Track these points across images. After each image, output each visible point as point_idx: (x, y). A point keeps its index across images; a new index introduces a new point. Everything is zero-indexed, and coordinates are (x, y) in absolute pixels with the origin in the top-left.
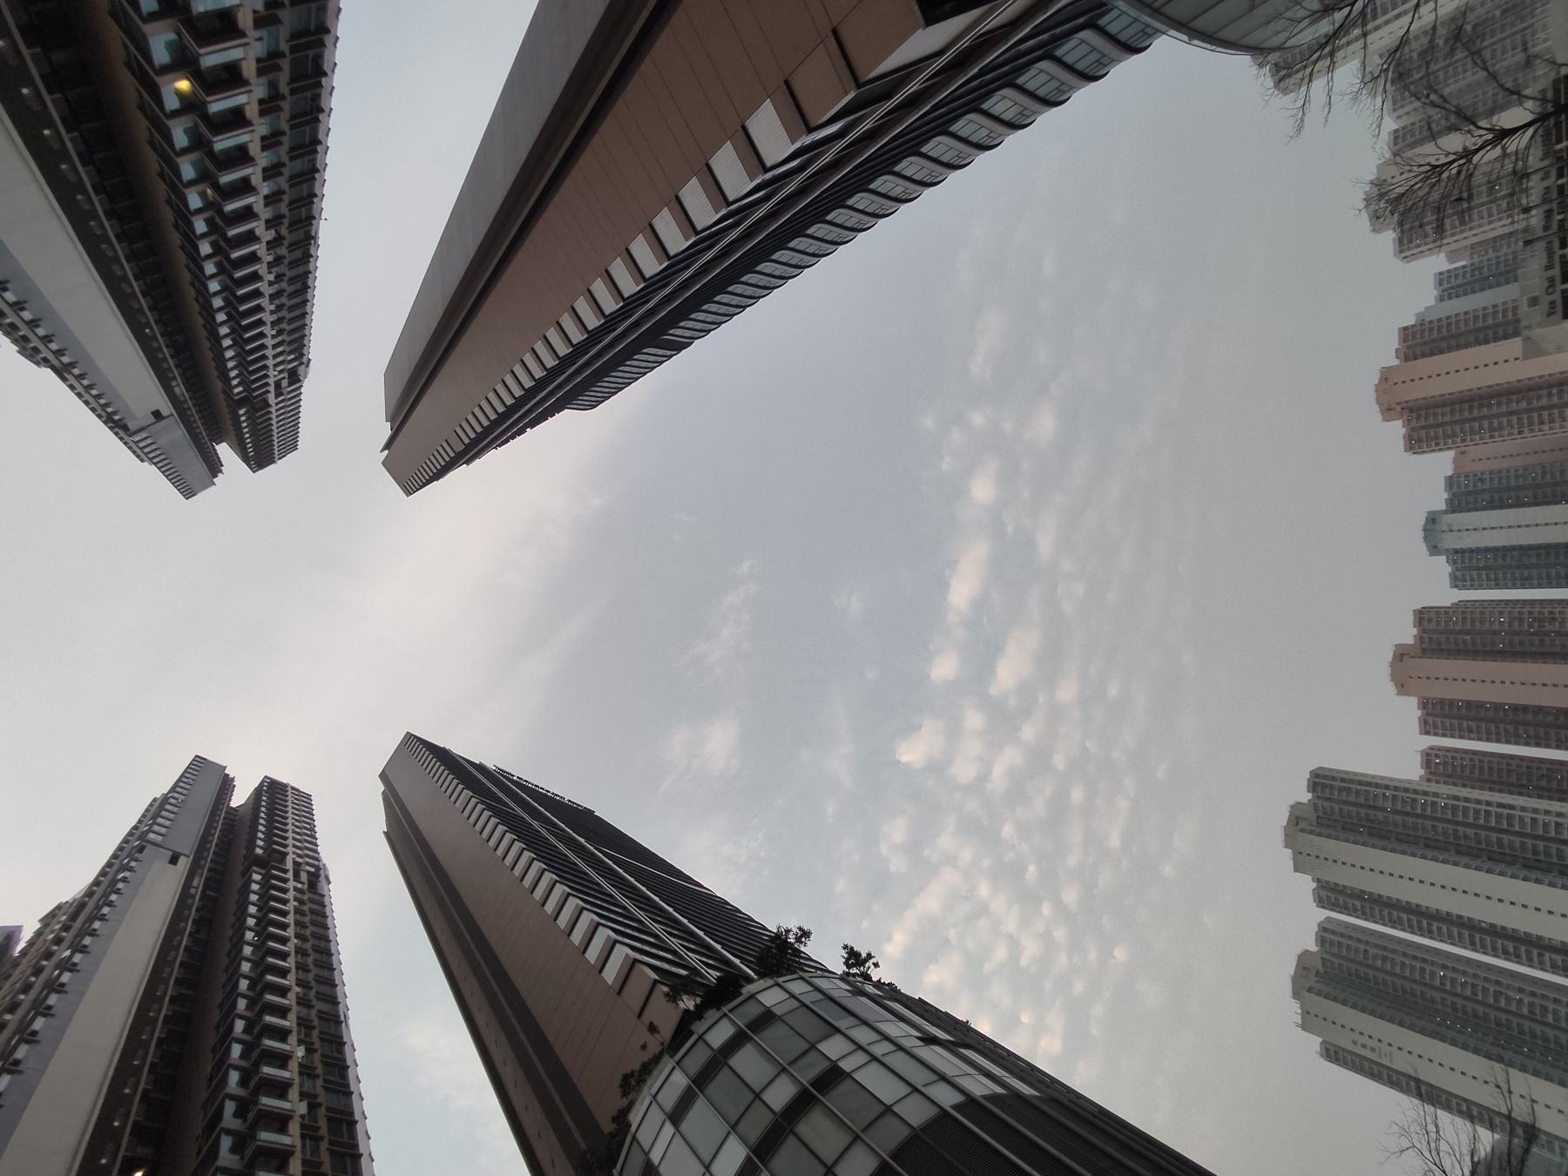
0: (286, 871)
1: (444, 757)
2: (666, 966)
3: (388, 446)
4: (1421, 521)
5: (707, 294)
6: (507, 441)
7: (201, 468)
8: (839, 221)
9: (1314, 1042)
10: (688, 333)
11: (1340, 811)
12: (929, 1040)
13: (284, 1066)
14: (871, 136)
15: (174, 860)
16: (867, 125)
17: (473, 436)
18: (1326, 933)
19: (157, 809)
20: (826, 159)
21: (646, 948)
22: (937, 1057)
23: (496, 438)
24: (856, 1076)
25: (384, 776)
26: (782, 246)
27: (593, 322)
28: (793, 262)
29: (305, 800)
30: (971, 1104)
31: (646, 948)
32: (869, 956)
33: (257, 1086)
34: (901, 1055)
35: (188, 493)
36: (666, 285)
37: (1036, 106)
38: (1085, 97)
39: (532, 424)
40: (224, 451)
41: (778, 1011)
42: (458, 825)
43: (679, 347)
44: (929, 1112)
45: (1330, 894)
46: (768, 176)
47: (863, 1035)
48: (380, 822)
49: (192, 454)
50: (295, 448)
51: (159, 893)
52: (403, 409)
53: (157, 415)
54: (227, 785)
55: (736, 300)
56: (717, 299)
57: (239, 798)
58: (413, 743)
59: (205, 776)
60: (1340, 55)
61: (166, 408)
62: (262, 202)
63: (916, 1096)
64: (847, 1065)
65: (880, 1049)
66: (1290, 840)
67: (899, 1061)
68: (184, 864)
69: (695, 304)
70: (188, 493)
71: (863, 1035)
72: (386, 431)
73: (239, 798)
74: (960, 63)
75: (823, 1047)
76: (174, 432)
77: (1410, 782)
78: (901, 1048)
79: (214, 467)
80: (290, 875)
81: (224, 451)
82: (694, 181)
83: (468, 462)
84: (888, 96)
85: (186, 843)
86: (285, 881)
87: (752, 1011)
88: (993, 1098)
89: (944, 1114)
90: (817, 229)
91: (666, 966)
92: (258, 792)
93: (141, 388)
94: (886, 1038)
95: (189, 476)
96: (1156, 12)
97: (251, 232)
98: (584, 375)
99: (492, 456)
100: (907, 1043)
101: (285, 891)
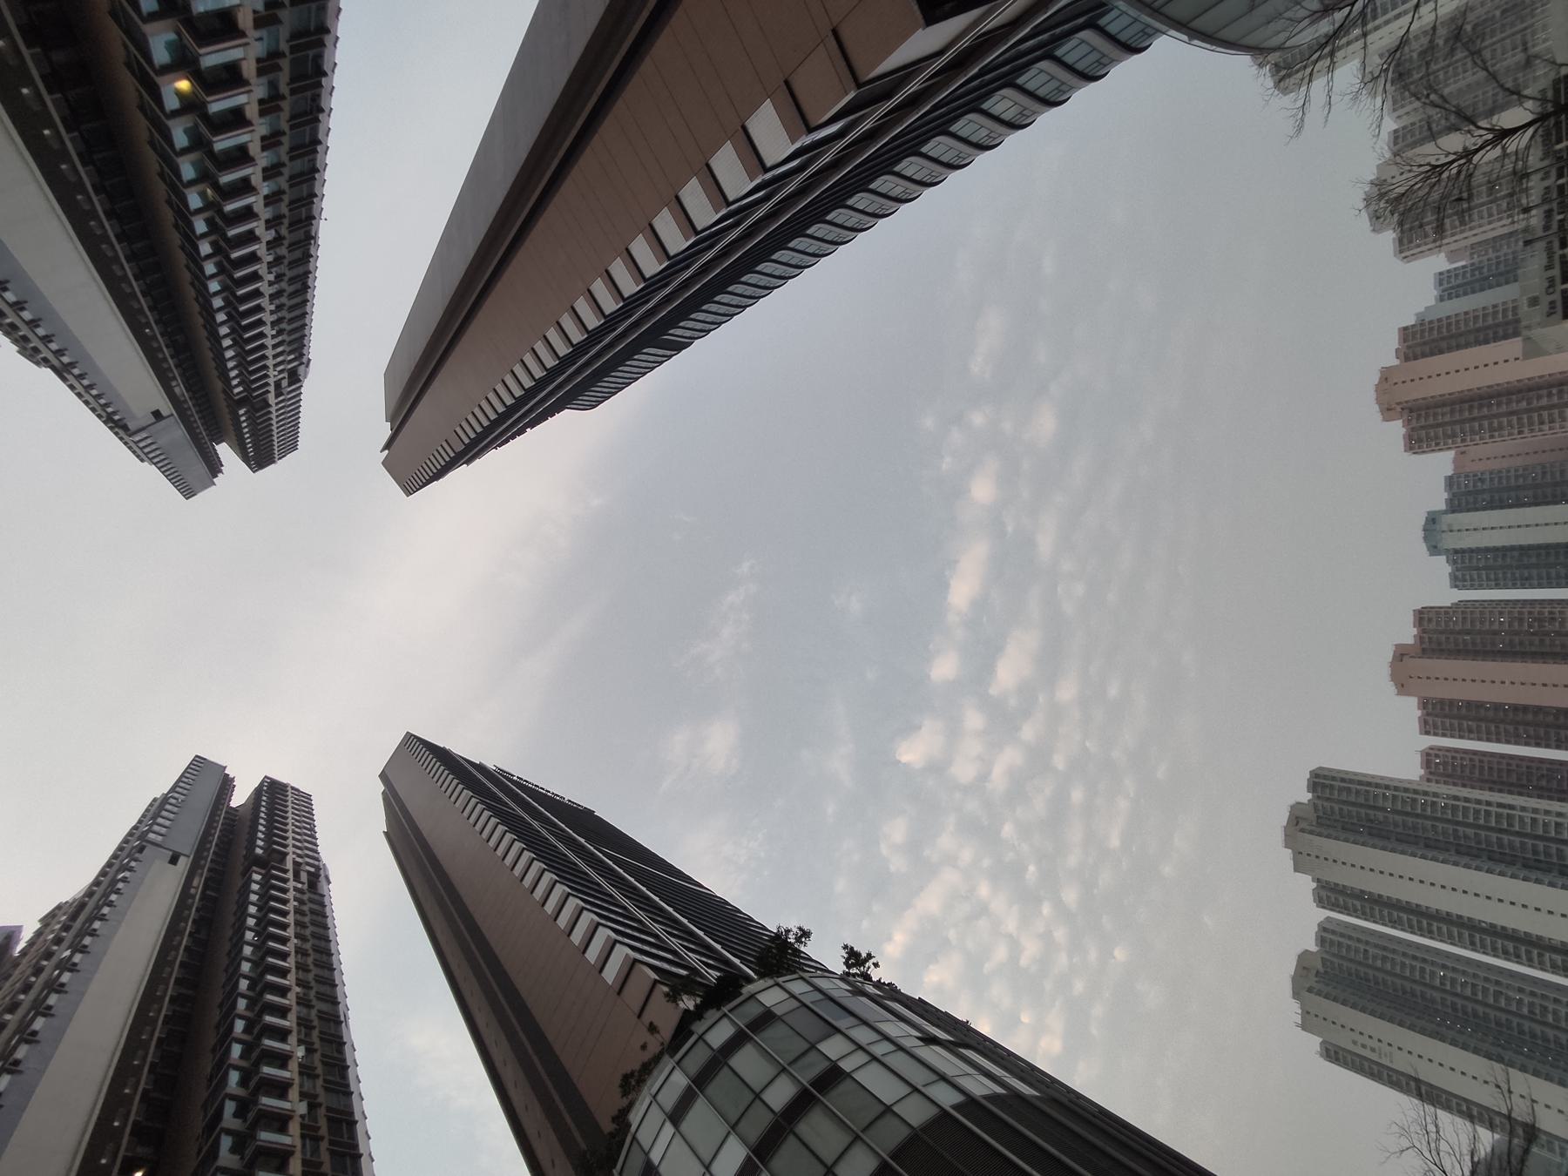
0: (286, 871)
1: (444, 757)
2: (666, 966)
3: (388, 446)
4: (1421, 521)
5: (707, 294)
6: (507, 441)
7: (201, 468)
8: (839, 221)
9: (1314, 1042)
10: (688, 333)
11: (1340, 811)
12: (929, 1040)
13: (284, 1066)
14: (871, 136)
15: (174, 860)
16: (867, 125)
17: (473, 436)
18: (1326, 933)
19: (157, 809)
20: (826, 159)
21: (646, 948)
22: (937, 1057)
23: (496, 438)
24: (856, 1076)
25: (384, 776)
26: (782, 246)
27: (593, 322)
28: (793, 262)
29: (305, 800)
30: (971, 1104)
31: (646, 948)
32: (869, 956)
33: (257, 1086)
34: (901, 1055)
35: (188, 493)
36: (666, 285)
37: (1036, 106)
38: (1085, 97)
39: (532, 424)
40: (224, 451)
41: (778, 1011)
42: (458, 825)
43: (679, 347)
44: (929, 1112)
45: (1330, 894)
46: (768, 176)
47: (863, 1035)
48: (380, 822)
49: (192, 454)
50: (295, 448)
51: (159, 893)
52: (403, 409)
53: (157, 415)
54: (227, 785)
55: (736, 300)
56: (717, 299)
57: (239, 798)
58: (413, 743)
59: (205, 776)
60: (1340, 55)
61: (166, 408)
62: (262, 202)
63: (916, 1096)
64: (847, 1065)
65: (880, 1049)
66: (1290, 840)
67: (899, 1061)
68: (184, 864)
69: (695, 304)
70: (188, 493)
71: (863, 1035)
72: (386, 431)
73: (239, 798)
74: (960, 63)
75: (823, 1047)
76: (174, 432)
77: (1410, 782)
78: (901, 1048)
79: (214, 467)
80: (290, 875)
81: (224, 451)
82: (694, 181)
83: (468, 462)
84: (888, 96)
85: (186, 843)
86: (285, 881)
87: (752, 1011)
88: (993, 1098)
89: (944, 1114)
90: (817, 229)
91: (666, 966)
92: (258, 792)
93: (141, 388)
94: (886, 1038)
95: (189, 476)
96: (1156, 12)
97: (251, 232)
98: (584, 375)
99: (492, 456)
100: (907, 1043)
101: (285, 891)
